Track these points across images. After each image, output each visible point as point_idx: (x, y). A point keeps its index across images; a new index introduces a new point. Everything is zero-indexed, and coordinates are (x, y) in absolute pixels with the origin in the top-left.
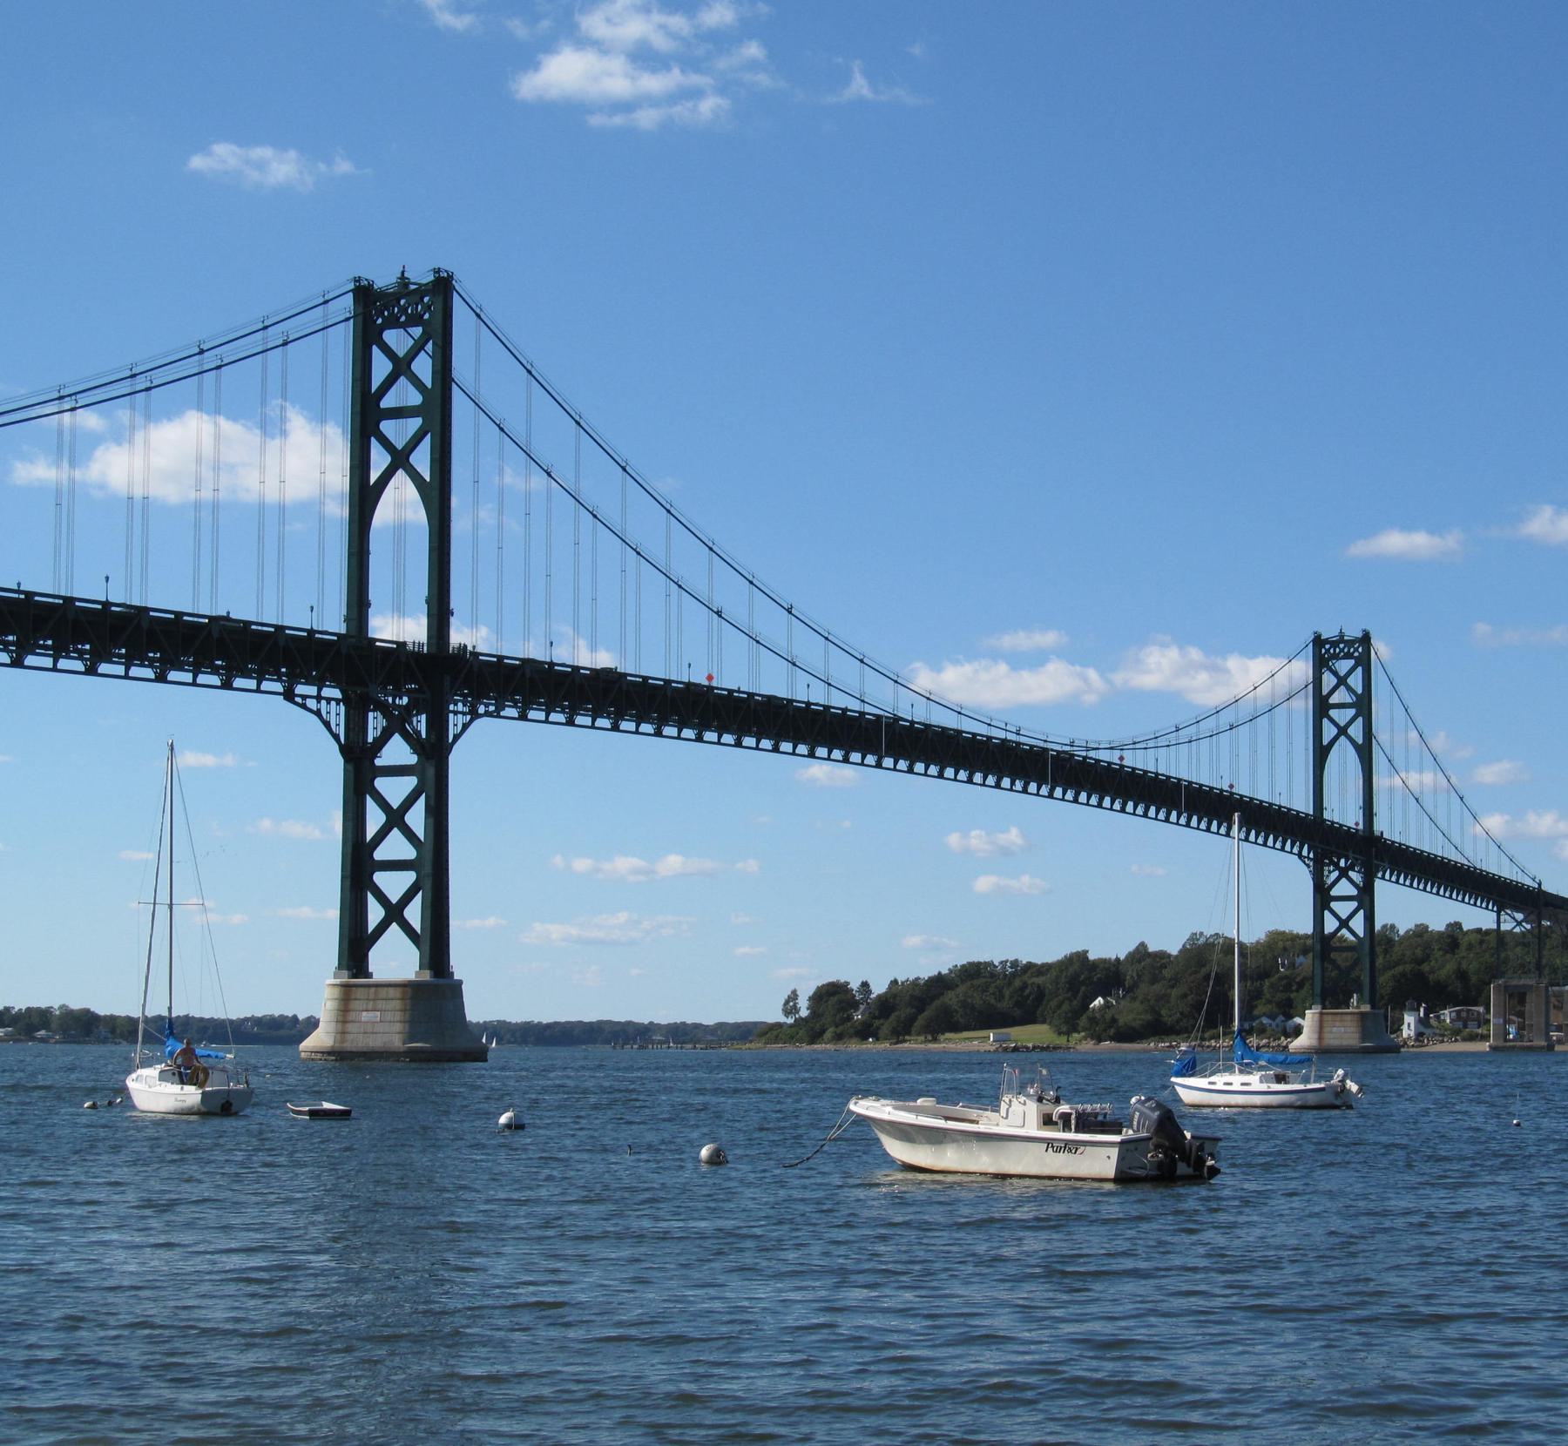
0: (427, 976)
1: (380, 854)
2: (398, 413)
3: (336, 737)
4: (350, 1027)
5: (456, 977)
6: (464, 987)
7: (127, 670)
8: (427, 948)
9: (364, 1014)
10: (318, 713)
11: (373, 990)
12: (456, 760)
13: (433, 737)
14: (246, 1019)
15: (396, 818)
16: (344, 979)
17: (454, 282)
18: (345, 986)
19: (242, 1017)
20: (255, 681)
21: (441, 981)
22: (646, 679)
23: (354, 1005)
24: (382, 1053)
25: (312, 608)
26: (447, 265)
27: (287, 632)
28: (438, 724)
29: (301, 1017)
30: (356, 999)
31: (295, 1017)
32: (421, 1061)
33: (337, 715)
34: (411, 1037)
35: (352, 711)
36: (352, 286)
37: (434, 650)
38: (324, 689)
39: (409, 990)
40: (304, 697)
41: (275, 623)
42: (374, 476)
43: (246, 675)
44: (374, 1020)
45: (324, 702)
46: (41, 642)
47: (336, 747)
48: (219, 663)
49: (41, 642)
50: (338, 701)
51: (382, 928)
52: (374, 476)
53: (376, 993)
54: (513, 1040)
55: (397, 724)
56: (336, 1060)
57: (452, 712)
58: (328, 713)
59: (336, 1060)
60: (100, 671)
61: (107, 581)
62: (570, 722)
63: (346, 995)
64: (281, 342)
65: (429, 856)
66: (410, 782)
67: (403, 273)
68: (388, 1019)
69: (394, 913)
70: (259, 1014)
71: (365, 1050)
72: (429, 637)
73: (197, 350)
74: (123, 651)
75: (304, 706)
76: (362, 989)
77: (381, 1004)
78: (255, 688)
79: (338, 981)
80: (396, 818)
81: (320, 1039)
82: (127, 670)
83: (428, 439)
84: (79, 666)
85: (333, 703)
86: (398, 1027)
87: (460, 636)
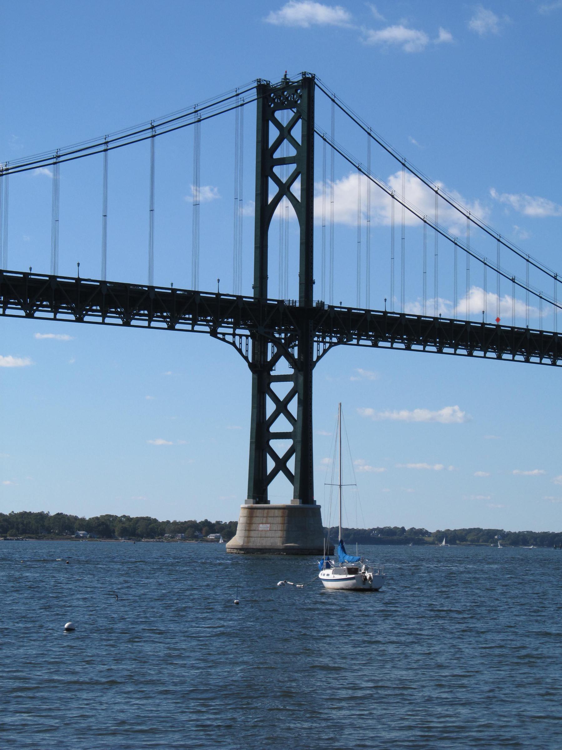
0: (297, 503)
1: (274, 429)
2: (283, 161)
3: (246, 358)
4: (253, 534)
5: (317, 504)
6: (322, 510)
7: (541, 360)
8: (298, 485)
9: (261, 525)
10: (233, 344)
11: (266, 511)
12: (316, 373)
13: (302, 357)
14: (374, 529)
15: (282, 407)
16: (251, 505)
17: (316, 80)
18: (251, 509)
19: (371, 528)
20: (422, 346)
21: (306, 506)
22: (541, 332)
23: (255, 520)
24: (270, 549)
25: (386, 300)
26: (310, 70)
27: (502, 328)
28: (306, 350)
29: (407, 528)
30: (257, 517)
31: (403, 528)
32: (293, 554)
33: (247, 345)
34: (287, 540)
35: (256, 343)
36: (255, 84)
37: (303, 305)
38: (58, 314)
39: (287, 511)
40: (224, 334)
41: (278, 299)
42: (270, 200)
43: (385, 340)
44: (266, 529)
45: (237, 338)
46: (226, 320)
47: (246, 364)
48: (371, 333)
49: (226, 320)
50: (247, 336)
51: (274, 473)
52: (270, 200)
53: (268, 513)
54: (534, 543)
55: (283, 351)
56: (244, 553)
57: (315, 341)
58: (241, 344)
59: (244, 553)
60: (503, 358)
61: (78, 266)
62: (527, 361)
63: (251, 513)
64: (196, 120)
65: (300, 430)
66: (290, 385)
67: (285, 75)
68: (275, 529)
69: (281, 464)
70: (382, 526)
71: (261, 548)
72: (300, 297)
73: (150, 126)
74: (191, 316)
75: (224, 340)
76: (260, 510)
77: (270, 520)
78: (53, 317)
79: (247, 506)
80: (282, 407)
81: (236, 541)
82: (541, 360)
83: (299, 178)
84: (402, 346)
85: (244, 338)
86: (279, 534)
87: (317, 296)
